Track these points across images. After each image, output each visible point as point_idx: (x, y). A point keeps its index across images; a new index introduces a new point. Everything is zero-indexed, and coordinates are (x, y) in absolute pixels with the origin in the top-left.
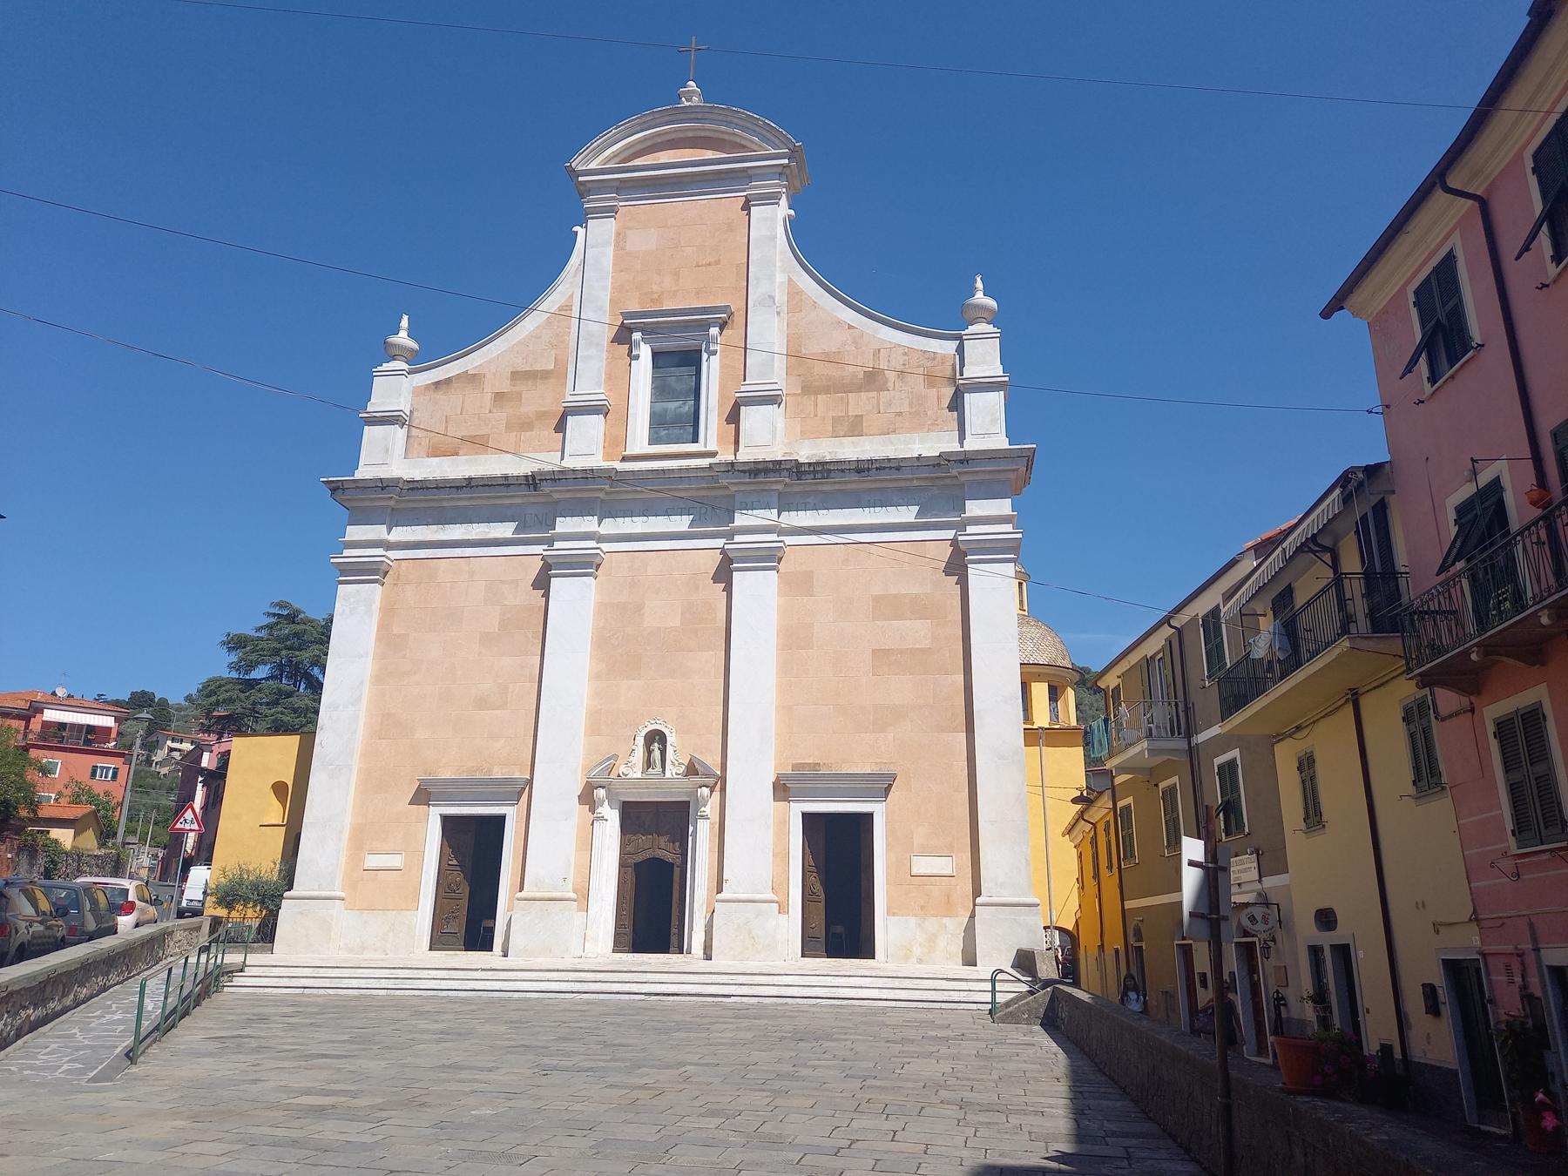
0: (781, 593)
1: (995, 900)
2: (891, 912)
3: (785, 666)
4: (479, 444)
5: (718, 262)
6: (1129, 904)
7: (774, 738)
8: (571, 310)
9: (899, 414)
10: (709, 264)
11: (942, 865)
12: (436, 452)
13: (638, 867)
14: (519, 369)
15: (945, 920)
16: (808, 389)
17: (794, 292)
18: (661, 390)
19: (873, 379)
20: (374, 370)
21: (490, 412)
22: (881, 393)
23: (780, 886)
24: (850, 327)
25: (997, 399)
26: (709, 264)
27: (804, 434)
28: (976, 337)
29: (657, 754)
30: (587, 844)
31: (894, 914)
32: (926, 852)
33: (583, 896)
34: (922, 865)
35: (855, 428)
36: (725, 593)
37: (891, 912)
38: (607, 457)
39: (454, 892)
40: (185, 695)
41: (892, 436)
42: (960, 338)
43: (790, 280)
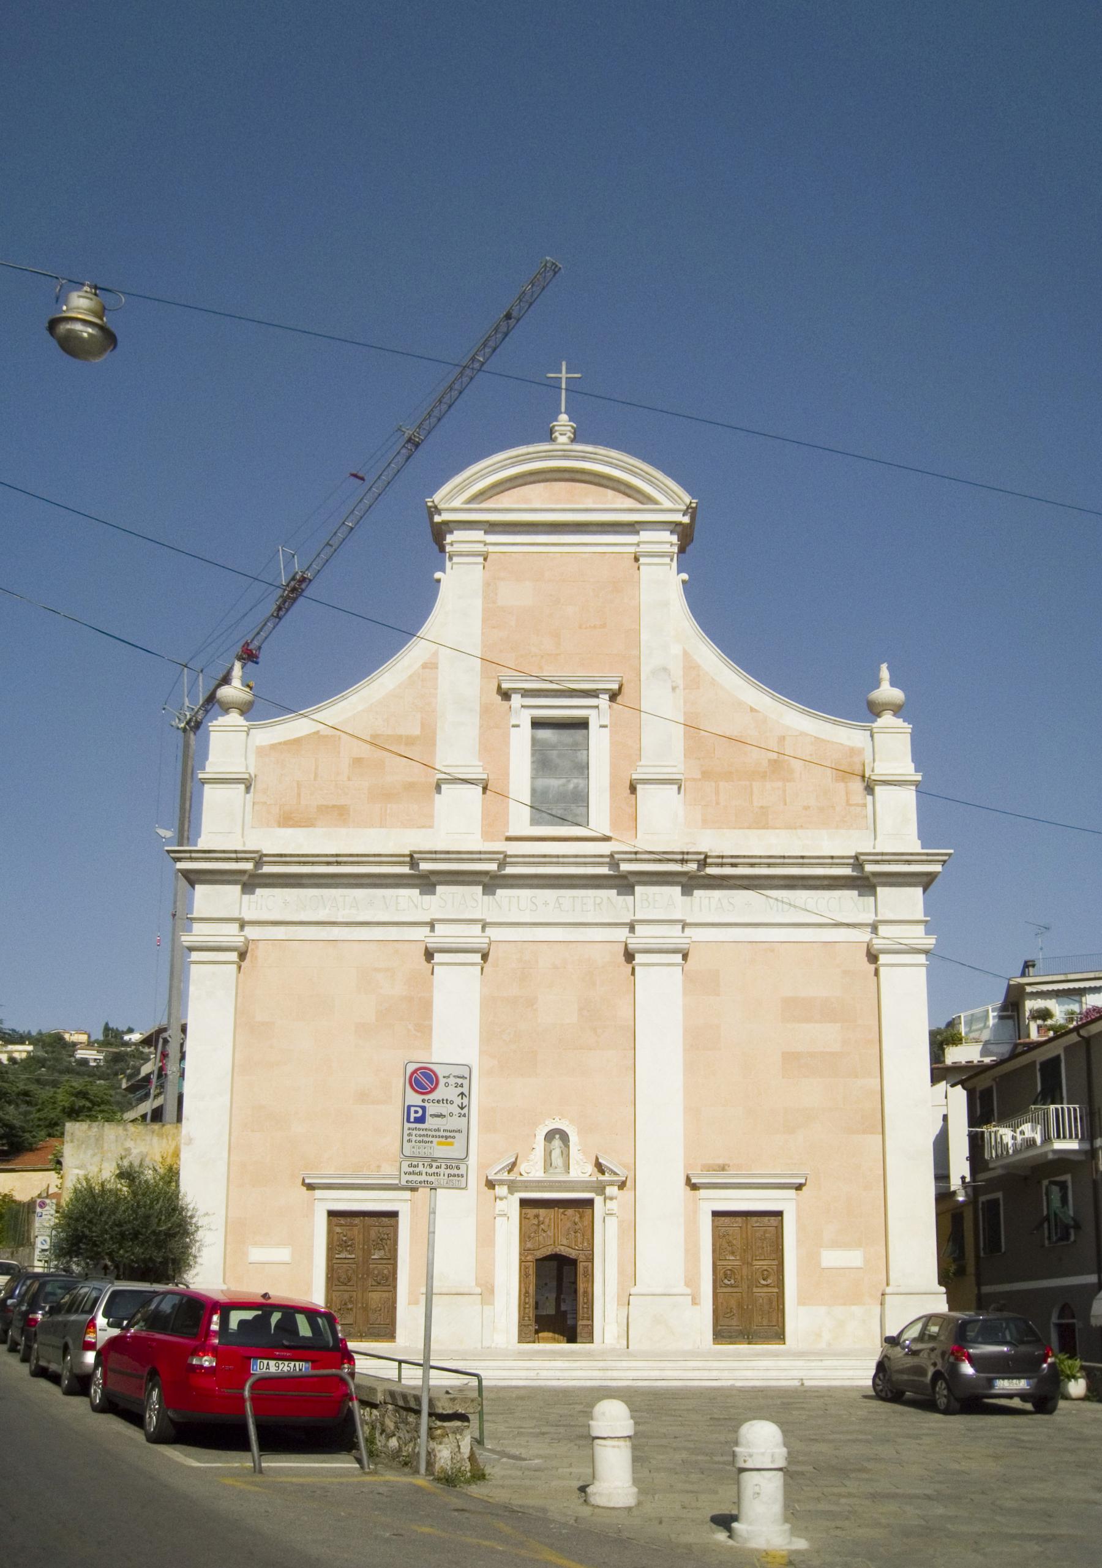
0: (686, 992)
1: (902, 1290)
2: (802, 1301)
3: (690, 1068)
4: (340, 814)
5: (604, 626)
6: (986, 1289)
7: (565, 1274)
8: (437, 668)
9: (806, 808)
10: (595, 627)
11: (831, 1258)
12: (287, 820)
13: (540, 1262)
14: (379, 732)
15: (854, 1308)
16: (706, 775)
17: (691, 667)
18: (542, 762)
19: (777, 767)
20: (210, 724)
21: (349, 779)
22: (787, 784)
23: (691, 1281)
24: (752, 710)
25: (908, 797)
26: (595, 627)
27: (705, 823)
28: (885, 730)
29: (556, 1154)
30: (486, 1239)
31: (804, 1304)
32: (835, 1245)
33: (487, 1293)
34: (831, 1258)
35: (761, 821)
36: (638, 889)
37: (802, 1301)
38: (487, 835)
39: (346, 1285)
40: (683, 1284)
41: (799, 831)
42: (871, 730)
43: (686, 654)
